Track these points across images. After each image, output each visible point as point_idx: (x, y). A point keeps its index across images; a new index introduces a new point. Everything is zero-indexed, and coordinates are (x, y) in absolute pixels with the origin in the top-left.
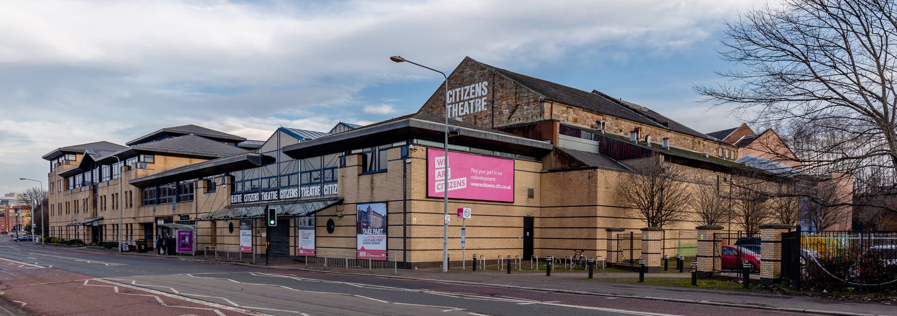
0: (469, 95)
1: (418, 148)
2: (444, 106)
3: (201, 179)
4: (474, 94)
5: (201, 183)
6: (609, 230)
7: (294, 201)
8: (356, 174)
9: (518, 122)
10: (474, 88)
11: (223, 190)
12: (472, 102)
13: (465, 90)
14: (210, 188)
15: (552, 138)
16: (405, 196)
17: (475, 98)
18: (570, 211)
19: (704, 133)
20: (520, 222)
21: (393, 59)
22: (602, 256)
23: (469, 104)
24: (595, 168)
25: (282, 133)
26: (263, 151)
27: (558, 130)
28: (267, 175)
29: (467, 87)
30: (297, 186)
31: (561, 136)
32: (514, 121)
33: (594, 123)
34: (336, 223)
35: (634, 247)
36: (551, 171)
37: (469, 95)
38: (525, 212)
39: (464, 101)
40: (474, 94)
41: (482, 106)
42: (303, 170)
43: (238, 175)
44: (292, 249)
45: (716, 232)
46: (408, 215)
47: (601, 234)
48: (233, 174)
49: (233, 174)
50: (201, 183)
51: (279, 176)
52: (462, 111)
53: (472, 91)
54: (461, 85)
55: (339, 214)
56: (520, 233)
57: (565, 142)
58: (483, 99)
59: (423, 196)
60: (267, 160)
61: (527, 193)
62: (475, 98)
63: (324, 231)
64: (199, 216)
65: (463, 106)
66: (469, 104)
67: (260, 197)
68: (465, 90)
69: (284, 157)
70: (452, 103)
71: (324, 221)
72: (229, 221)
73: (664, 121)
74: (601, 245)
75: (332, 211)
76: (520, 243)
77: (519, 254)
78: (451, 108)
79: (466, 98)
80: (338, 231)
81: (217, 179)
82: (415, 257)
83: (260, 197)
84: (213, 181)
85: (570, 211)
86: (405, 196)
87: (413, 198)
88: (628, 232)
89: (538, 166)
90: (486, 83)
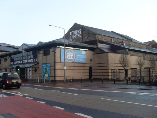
0: (76, 33)
1: (58, 48)
2: (70, 36)
3: (3, 58)
4: (77, 32)
5: (3, 59)
6: (111, 70)
7: (26, 63)
8: (42, 56)
9: (89, 40)
10: (77, 31)
11: (9, 61)
12: (77, 35)
13: (75, 32)
14: (5, 60)
15: (96, 44)
16: (55, 62)
17: (78, 34)
18: (102, 65)
19: (143, 42)
20: (88, 68)
21: (50, 26)
22: (110, 77)
23: (76, 35)
24: (108, 53)
25: (24, 45)
26: (19, 50)
27: (98, 43)
28: (20, 56)
29: (76, 31)
30: (27, 59)
31: (99, 44)
32: (88, 40)
33: (111, 40)
34: (37, 69)
35: (54, 74)
36: (97, 54)
37: (76, 33)
38: (89, 65)
39: (75, 35)
40: (77, 32)
41: (79, 36)
42: (19, 57)
43: (12, 56)
44: (26, 77)
45: (114, 71)
46: (55, 67)
47: (110, 71)
48: (11, 56)
49: (11, 56)
50: (3, 59)
51: (23, 57)
52: (74, 37)
53: (77, 32)
54: (74, 30)
55: (38, 67)
56: (88, 71)
57: (100, 46)
58: (80, 34)
59: (59, 62)
60: (20, 52)
61: (90, 60)
62: (78, 34)
63: (34, 72)
64: (2, 68)
65: (74, 36)
66: (76, 35)
67: (18, 62)
68: (75, 32)
69: (24, 51)
70: (71, 35)
71: (34, 69)
72: (10, 69)
73: (130, 39)
74: (110, 74)
75: (36, 66)
76: (88, 74)
77: (88, 77)
78: (71, 37)
79: (75, 34)
80: (38, 72)
81: (7, 58)
82: (58, 79)
83: (18, 62)
84: (6, 58)
85: (102, 65)
86: (55, 62)
87: (57, 62)
88: (116, 70)
89: (93, 52)
90: (80, 30)
